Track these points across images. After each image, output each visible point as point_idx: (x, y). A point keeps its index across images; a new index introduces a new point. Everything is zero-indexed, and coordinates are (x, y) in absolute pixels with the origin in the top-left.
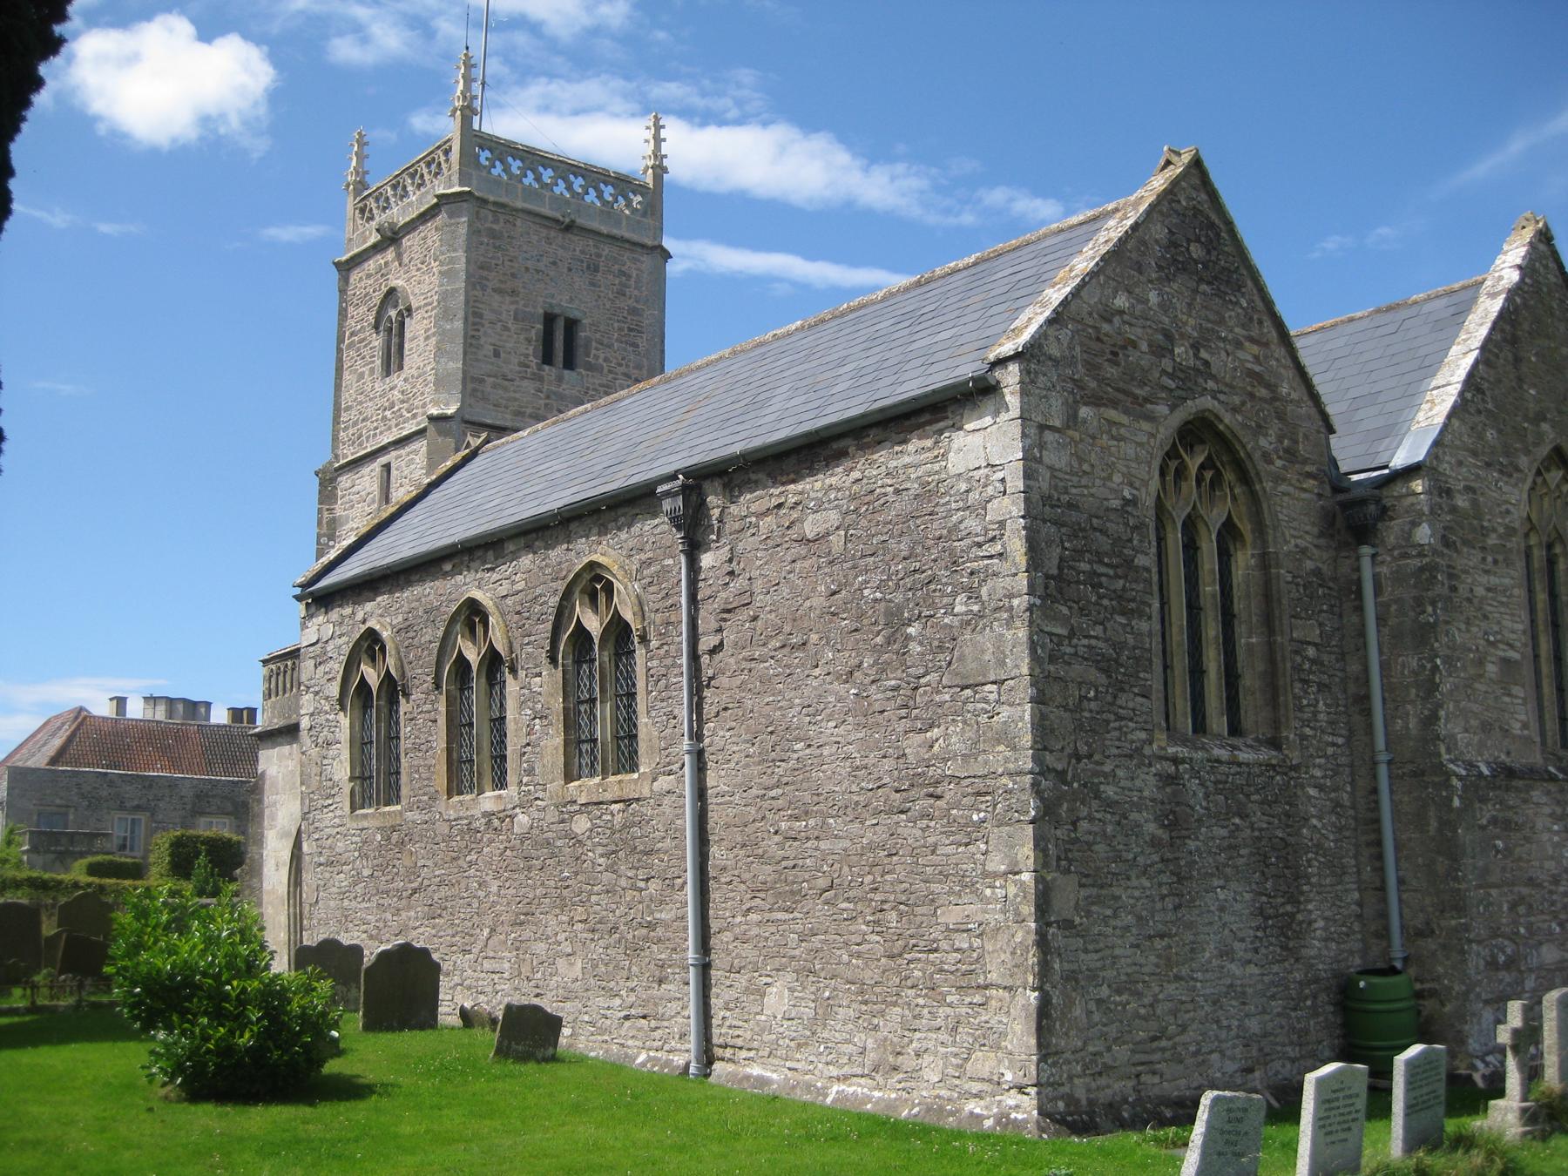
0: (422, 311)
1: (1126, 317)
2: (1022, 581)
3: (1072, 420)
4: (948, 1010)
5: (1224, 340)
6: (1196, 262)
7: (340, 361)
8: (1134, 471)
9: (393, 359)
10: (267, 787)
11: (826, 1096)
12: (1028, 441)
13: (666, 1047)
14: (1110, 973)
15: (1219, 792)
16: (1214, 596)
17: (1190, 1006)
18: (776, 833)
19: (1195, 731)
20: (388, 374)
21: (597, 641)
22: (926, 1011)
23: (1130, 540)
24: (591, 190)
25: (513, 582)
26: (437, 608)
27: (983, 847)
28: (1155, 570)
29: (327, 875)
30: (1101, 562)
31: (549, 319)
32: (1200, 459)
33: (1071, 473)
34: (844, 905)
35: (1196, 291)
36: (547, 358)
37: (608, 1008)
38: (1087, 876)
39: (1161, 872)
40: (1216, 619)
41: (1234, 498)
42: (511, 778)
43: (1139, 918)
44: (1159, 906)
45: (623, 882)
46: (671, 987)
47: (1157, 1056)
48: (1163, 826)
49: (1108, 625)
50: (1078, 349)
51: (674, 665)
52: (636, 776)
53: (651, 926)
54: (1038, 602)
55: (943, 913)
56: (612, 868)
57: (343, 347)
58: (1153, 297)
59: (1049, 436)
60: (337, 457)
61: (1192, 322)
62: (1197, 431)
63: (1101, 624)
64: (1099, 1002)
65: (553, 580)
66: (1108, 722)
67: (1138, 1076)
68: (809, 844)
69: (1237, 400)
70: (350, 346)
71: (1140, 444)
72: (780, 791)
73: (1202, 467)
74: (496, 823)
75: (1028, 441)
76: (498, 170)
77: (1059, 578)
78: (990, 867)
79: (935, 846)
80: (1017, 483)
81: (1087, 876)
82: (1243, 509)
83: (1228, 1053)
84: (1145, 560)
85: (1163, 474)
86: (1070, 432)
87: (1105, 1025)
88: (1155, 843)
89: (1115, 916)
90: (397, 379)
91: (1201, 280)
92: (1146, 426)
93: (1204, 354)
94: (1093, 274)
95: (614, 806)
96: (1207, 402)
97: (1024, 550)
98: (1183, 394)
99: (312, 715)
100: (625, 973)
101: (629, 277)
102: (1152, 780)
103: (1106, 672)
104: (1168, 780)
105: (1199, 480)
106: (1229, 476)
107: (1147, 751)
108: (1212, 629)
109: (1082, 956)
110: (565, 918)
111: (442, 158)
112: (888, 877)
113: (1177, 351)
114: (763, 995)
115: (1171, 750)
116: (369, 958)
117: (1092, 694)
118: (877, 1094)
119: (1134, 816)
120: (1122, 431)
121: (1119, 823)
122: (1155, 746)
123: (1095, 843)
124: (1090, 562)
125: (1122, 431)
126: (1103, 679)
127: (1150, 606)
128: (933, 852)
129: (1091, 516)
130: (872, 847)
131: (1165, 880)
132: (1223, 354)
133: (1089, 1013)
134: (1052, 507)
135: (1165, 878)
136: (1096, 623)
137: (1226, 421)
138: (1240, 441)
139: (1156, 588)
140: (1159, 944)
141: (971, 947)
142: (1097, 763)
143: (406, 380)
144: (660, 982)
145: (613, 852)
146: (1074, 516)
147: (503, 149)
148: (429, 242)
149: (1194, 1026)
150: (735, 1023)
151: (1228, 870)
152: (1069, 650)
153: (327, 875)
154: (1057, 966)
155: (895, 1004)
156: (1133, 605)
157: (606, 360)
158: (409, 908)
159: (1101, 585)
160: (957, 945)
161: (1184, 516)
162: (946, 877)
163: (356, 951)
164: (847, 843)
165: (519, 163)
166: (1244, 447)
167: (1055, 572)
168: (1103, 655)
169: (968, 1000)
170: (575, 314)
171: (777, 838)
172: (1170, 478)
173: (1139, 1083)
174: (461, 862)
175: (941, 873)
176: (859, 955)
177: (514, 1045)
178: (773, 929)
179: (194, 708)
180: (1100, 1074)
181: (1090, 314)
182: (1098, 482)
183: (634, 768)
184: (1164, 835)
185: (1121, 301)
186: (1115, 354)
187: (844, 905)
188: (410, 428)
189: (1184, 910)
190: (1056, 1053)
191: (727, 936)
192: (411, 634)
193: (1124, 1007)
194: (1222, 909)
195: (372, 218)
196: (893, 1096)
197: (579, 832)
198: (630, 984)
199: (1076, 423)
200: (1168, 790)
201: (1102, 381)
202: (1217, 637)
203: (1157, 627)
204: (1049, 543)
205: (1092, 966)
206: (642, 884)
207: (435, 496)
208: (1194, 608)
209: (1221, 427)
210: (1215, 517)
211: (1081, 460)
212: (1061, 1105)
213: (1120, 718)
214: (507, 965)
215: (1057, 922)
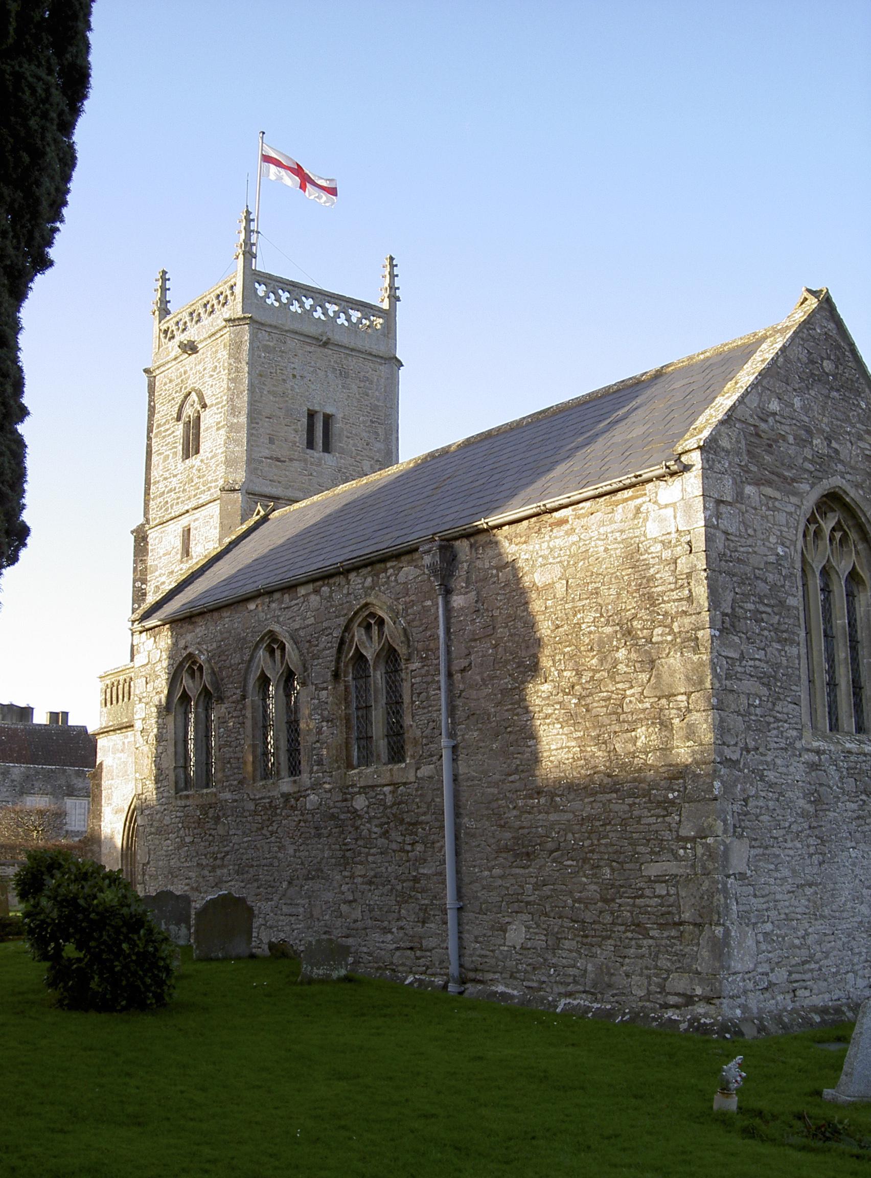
0: (214, 408)
1: (777, 418)
2: (706, 616)
3: (740, 497)
4: (651, 941)
5: (849, 433)
6: (828, 375)
7: (149, 446)
8: (784, 534)
9: (191, 446)
10: (104, 774)
11: (556, 1007)
12: (709, 513)
13: (429, 971)
14: (773, 914)
15: (850, 775)
16: (844, 628)
17: (832, 938)
18: (514, 808)
19: (831, 730)
20: (188, 457)
21: (371, 663)
22: (633, 942)
23: (783, 586)
24: (308, 308)
25: (304, 619)
26: (244, 638)
27: (677, 818)
28: (801, 608)
29: (157, 842)
30: (762, 603)
31: (311, 415)
32: (832, 524)
33: (740, 536)
34: (570, 863)
35: (828, 397)
36: (310, 444)
37: (383, 942)
38: (756, 840)
39: (809, 836)
40: (845, 645)
41: (857, 553)
42: (304, 766)
43: (794, 871)
44: (808, 862)
45: (394, 846)
46: (432, 925)
47: (808, 976)
48: (810, 802)
49: (768, 650)
50: (743, 442)
51: (433, 682)
52: (403, 765)
53: (416, 880)
54: (717, 633)
55: (646, 868)
56: (385, 834)
57: (152, 435)
58: (797, 403)
59: (723, 509)
60: (147, 521)
61: (825, 420)
62: (833, 500)
63: (763, 649)
64: (766, 934)
65: (337, 617)
66: (769, 723)
67: (794, 991)
68: (540, 817)
69: (859, 479)
70: (156, 436)
71: (790, 514)
72: (517, 777)
73: (833, 529)
74: (293, 801)
75: (709, 513)
76: (342, 320)
77: (733, 616)
78: (683, 833)
79: (640, 817)
80: (700, 544)
81: (756, 840)
82: (864, 561)
83: (860, 973)
84: (795, 601)
85: (805, 536)
86: (738, 505)
87: (770, 952)
88: (804, 814)
89: (777, 870)
90: (194, 461)
91: (832, 388)
92: (794, 500)
93: (834, 444)
94: (753, 386)
95: (385, 789)
96: (836, 481)
97: (706, 595)
98: (820, 474)
99: (143, 719)
100: (396, 915)
101: (371, 383)
102: (802, 767)
103: (767, 685)
104: (813, 767)
105: (831, 540)
106: (853, 536)
107: (798, 745)
108: (842, 653)
109: (753, 900)
110: (346, 874)
111: (228, 293)
112: (603, 841)
113: (815, 442)
114: (505, 931)
115: (815, 744)
116: (198, 905)
117: (757, 702)
118: (596, 1005)
119: (789, 794)
120: (777, 504)
121: (778, 800)
122: (803, 742)
123: (761, 815)
124: (754, 603)
125: (777, 504)
126: (764, 691)
127: (798, 635)
128: (638, 822)
129: (754, 568)
130: (590, 818)
131: (812, 843)
132: (849, 444)
133: (758, 942)
134: (726, 561)
135: (811, 841)
136: (759, 649)
137: (852, 495)
138: (862, 511)
139: (802, 621)
140: (809, 891)
141: (668, 894)
142: (762, 754)
143: (202, 461)
144: (424, 922)
145: (386, 823)
146: (740, 569)
147: (275, 283)
148: (219, 355)
149: (835, 953)
150: (483, 952)
151: (858, 834)
152: (740, 669)
153: (157, 842)
154: (734, 908)
155: (609, 937)
156: (785, 635)
157: (354, 445)
158: (222, 866)
159: (762, 620)
160: (658, 892)
161: (820, 568)
162: (648, 841)
163: (186, 900)
164: (571, 816)
165: (287, 295)
166: (865, 515)
167: (729, 611)
168: (764, 673)
169: (666, 934)
170: (329, 410)
171: (515, 812)
172: (810, 538)
173: (795, 996)
174: (264, 832)
175: (644, 838)
176: (579, 901)
177: (315, 970)
178: (513, 881)
179: (26, 712)
180: (766, 989)
181: (751, 416)
182: (759, 543)
183: (402, 760)
184: (811, 809)
185: (774, 406)
186: (770, 446)
187: (570, 863)
188: (204, 498)
189: (826, 866)
190: (734, 974)
191: (476, 886)
192: (224, 658)
193: (784, 939)
194: (854, 864)
195: (173, 337)
196: (609, 1007)
197: (358, 808)
198: (401, 923)
199: (742, 498)
200: (813, 774)
201: (762, 466)
202: (846, 658)
203: (803, 651)
204: (725, 589)
205: (760, 907)
206: (409, 848)
207: (235, 552)
208: (828, 636)
209: (847, 499)
210: (843, 567)
211: (747, 527)
212: (738, 1012)
213: (777, 720)
214: (301, 910)
215: (734, 874)
